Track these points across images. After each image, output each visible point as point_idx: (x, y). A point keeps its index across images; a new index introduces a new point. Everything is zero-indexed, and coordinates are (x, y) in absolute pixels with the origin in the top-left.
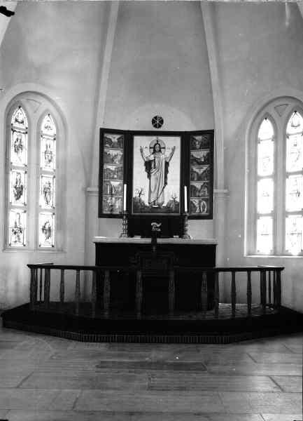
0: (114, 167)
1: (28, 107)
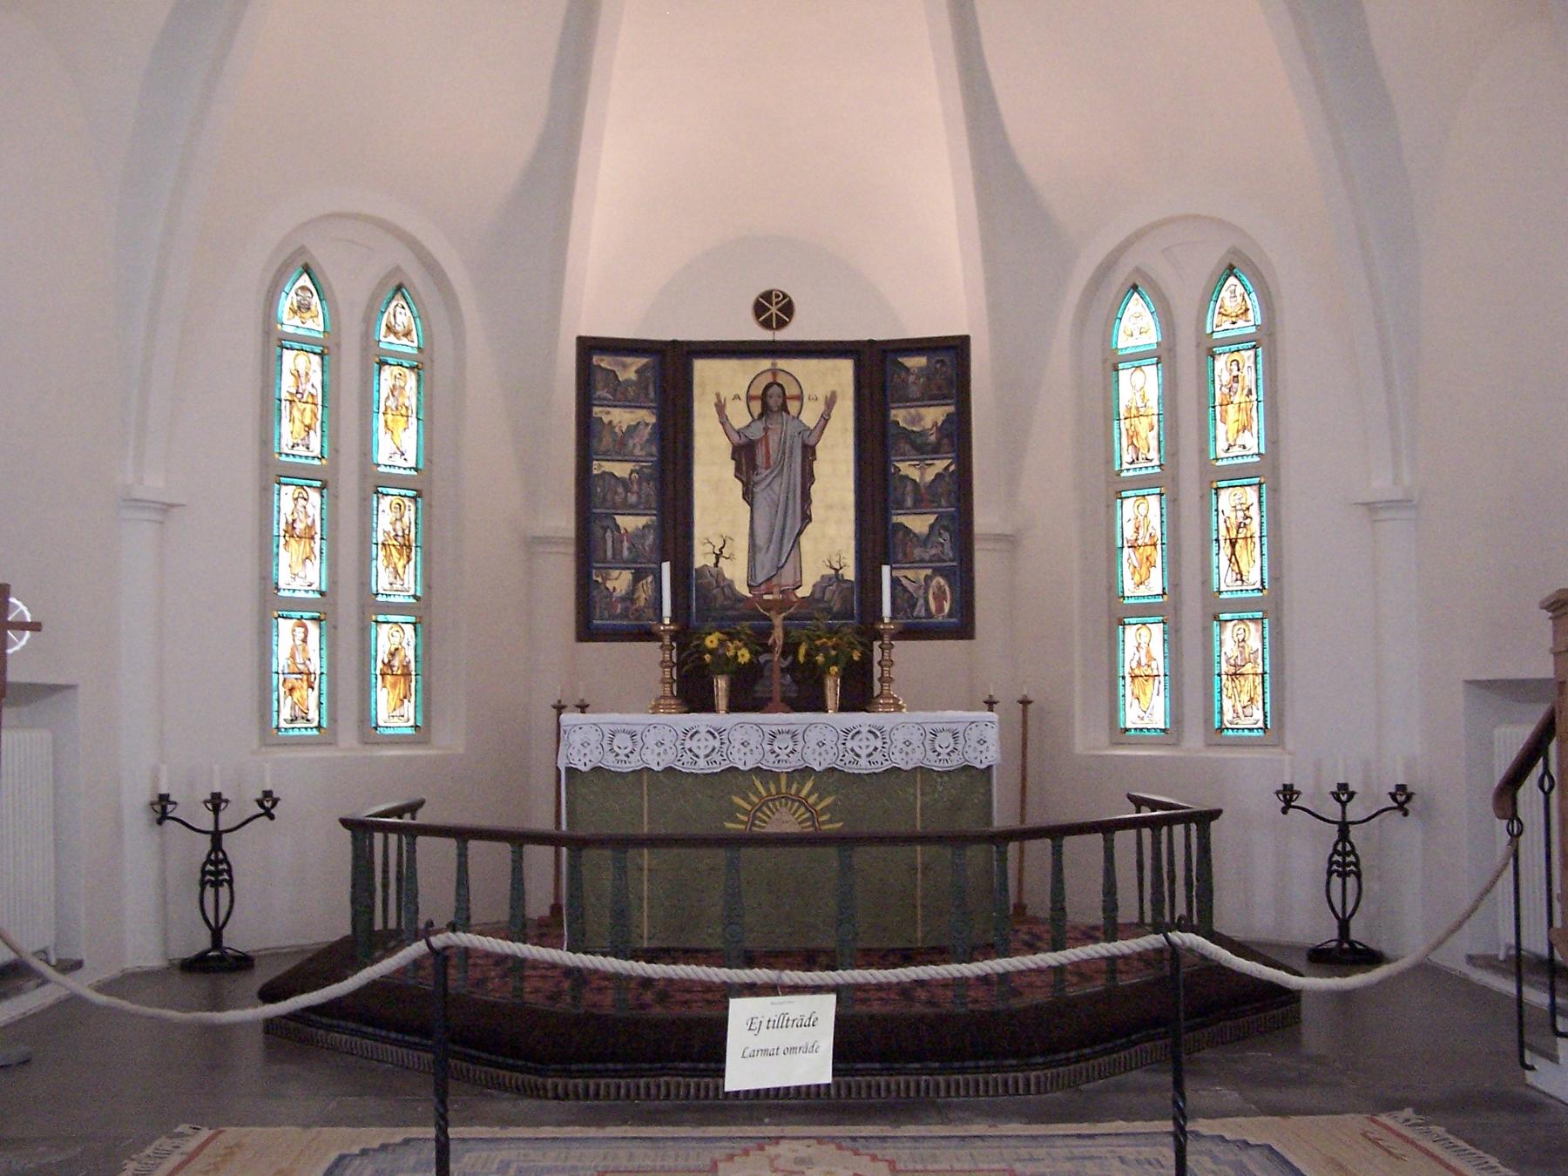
0: (629, 466)
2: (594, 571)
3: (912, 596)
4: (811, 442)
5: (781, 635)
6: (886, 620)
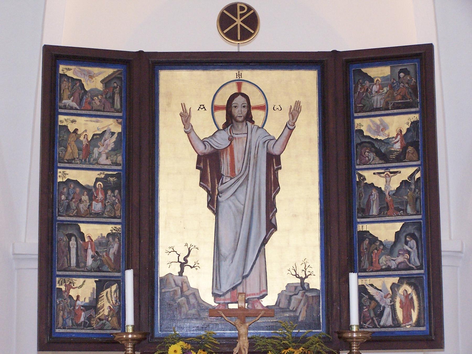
0: (94, 175)
1: (11, 251)
2: (57, 279)
3: (378, 305)
4: (276, 151)
5: (246, 344)
6: (355, 329)
